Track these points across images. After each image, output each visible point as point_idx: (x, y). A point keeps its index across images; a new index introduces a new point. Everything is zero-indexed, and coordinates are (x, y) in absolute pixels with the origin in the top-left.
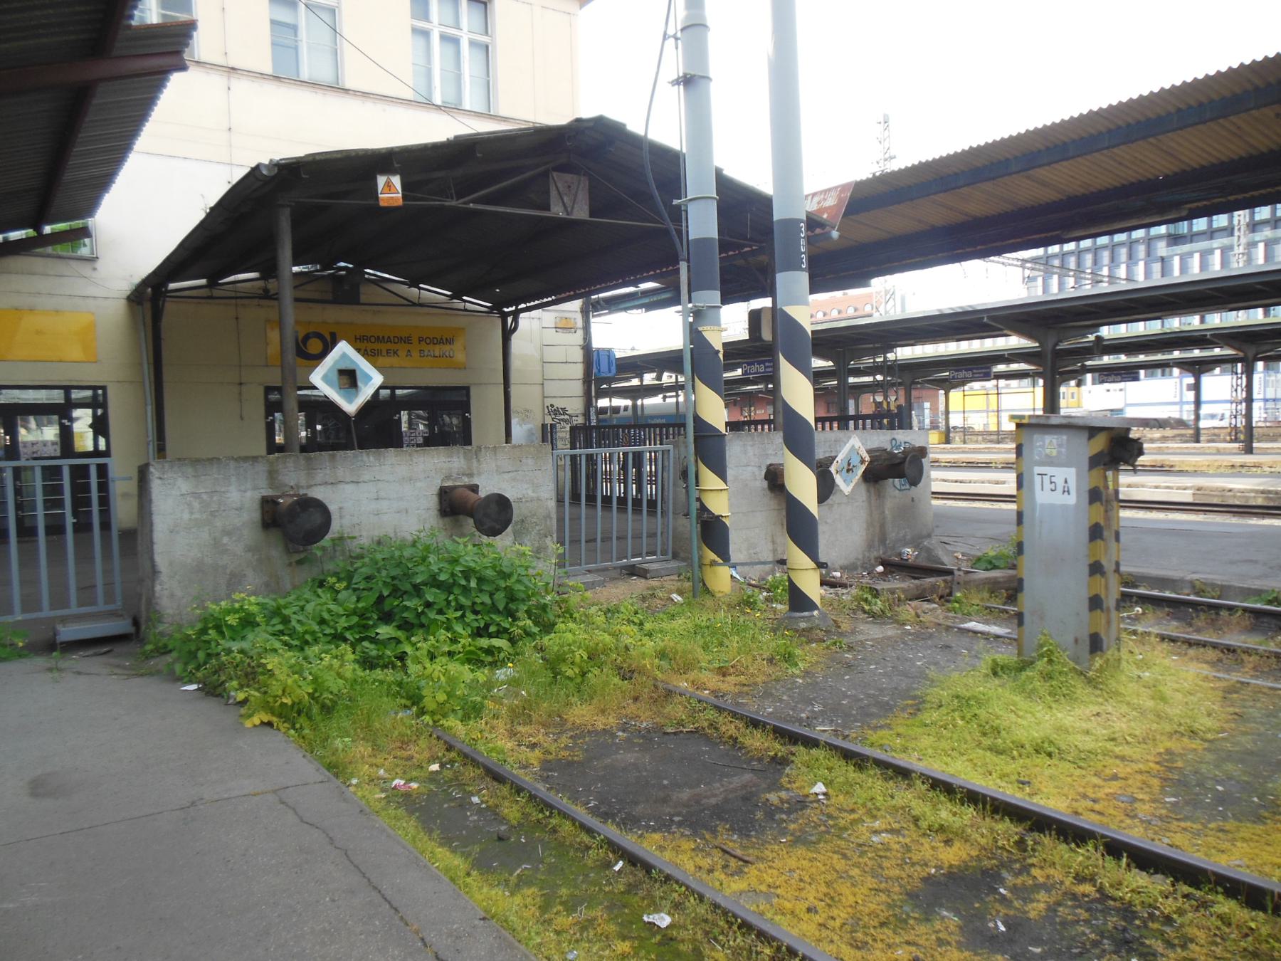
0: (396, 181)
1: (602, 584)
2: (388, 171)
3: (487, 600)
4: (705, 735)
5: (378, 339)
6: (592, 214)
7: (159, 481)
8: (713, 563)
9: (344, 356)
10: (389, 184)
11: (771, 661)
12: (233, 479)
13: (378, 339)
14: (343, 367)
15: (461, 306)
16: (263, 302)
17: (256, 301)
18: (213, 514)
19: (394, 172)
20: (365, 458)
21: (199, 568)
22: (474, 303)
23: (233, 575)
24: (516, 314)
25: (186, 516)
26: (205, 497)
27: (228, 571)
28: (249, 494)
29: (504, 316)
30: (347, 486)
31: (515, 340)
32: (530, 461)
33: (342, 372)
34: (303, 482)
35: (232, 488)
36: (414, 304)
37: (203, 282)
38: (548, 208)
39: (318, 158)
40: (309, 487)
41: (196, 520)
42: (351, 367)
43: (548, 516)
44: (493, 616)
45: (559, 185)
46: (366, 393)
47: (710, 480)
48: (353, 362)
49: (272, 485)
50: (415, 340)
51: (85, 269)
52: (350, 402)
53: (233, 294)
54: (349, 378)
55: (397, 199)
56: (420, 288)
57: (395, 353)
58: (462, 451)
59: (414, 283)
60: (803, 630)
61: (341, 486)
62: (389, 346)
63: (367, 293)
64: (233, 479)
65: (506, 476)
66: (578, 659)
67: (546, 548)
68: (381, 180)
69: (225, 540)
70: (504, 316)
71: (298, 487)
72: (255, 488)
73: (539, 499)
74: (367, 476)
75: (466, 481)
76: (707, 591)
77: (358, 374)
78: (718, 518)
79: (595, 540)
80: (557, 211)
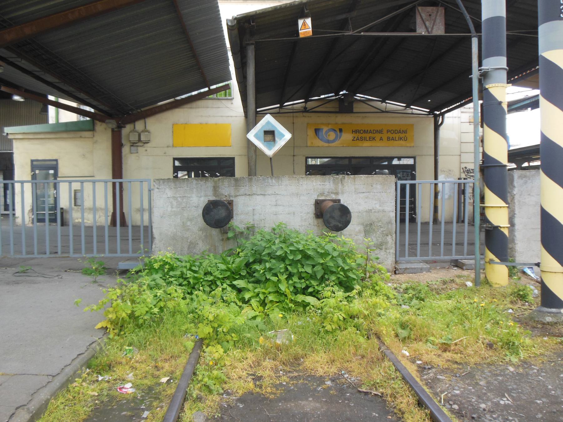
0: (309, 21)
1: (429, 270)
2: (304, 16)
3: (309, 270)
4: (385, 401)
5: (365, 132)
6: (446, 33)
7: (157, 190)
8: (491, 261)
9: (268, 123)
10: (304, 24)
11: (490, 346)
12: (195, 190)
13: (365, 132)
14: (267, 129)
15: (410, 111)
16: (305, 114)
17: (301, 114)
18: (183, 209)
19: (306, 16)
20: (270, 181)
21: (174, 238)
22: (416, 109)
23: (191, 243)
24: (443, 114)
25: (169, 209)
26: (179, 199)
27: (189, 241)
28: (202, 199)
29: (436, 117)
30: (258, 197)
31: (442, 131)
32: (379, 186)
33: (267, 133)
34: (233, 193)
35: (194, 195)
36: (383, 112)
37: (278, 105)
38: (415, 31)
39: (258, 12)
40: (236, 196)
41: (175, 211)
42: (272, 129)
43: (390, 222)
44: (312, 282)
45: (423, 15)
46: (281, 143)
47: (492, 199)
48: (273, 126)
49: (215, 194)
50: (385, 131)
51: (230, 102)
52: (270, 149)
53: (292, 111)
54: (270, 134)
55: (309, 32)
56: (412, 109)
57: (374, 139)
58: (332, 178)
59: (383, 101)
60: (548, 323)
61: (254, 197)
62: (371, 135)
63: (357, 107)
64: (195, 190)
65: (362, 195)
66: (335, 319)
67: (387, 243)
68: (300, 22)
69: (189, 223)
70: (436, 117)
71: (230, 196)
72: (206, 196)
73: (384, 211)
74: (270, 191)
75: (334, 197)
76: (487, 282)
77: (276, 133)
78: (497, 227)
79: (462, 244)
80: (421, 31)
